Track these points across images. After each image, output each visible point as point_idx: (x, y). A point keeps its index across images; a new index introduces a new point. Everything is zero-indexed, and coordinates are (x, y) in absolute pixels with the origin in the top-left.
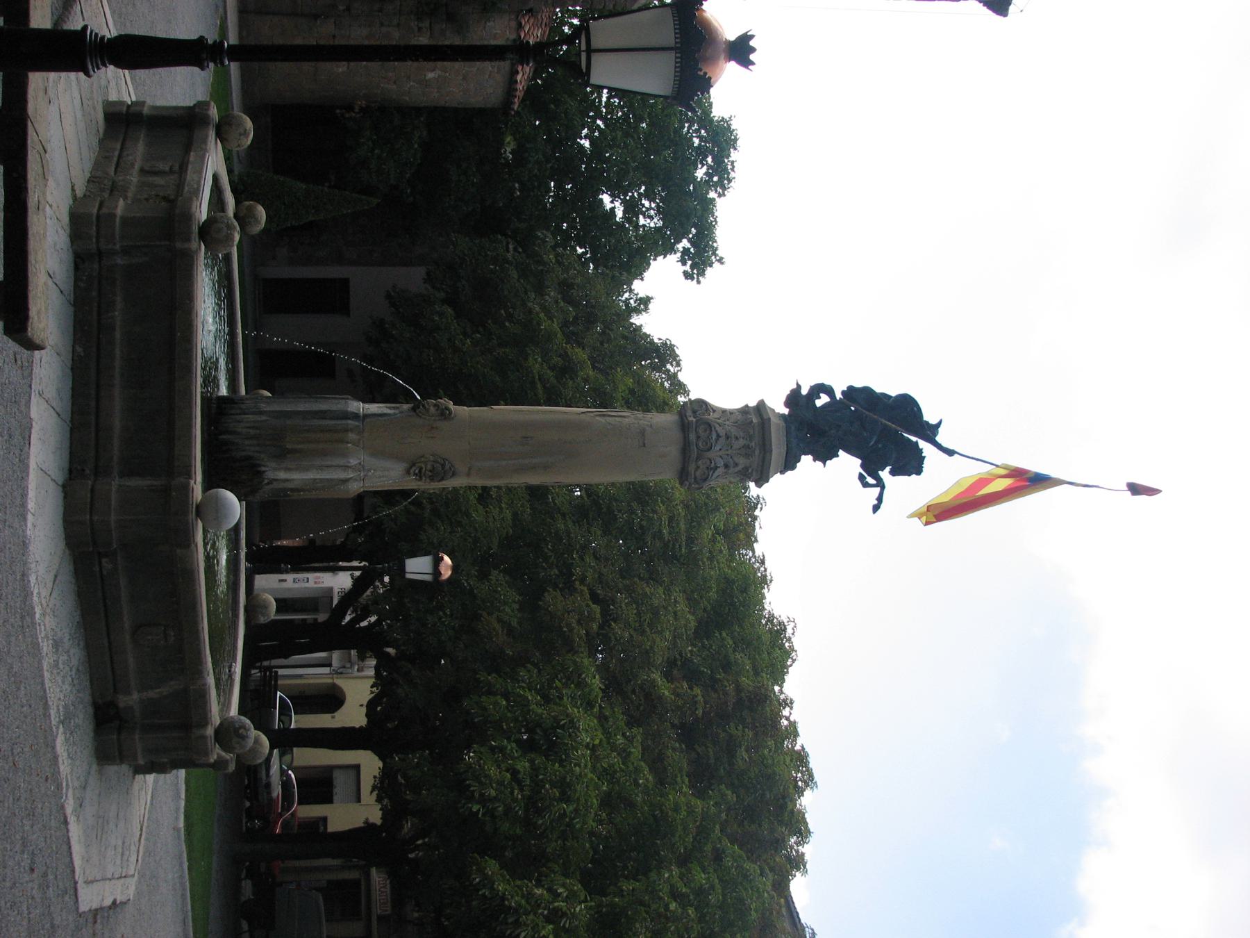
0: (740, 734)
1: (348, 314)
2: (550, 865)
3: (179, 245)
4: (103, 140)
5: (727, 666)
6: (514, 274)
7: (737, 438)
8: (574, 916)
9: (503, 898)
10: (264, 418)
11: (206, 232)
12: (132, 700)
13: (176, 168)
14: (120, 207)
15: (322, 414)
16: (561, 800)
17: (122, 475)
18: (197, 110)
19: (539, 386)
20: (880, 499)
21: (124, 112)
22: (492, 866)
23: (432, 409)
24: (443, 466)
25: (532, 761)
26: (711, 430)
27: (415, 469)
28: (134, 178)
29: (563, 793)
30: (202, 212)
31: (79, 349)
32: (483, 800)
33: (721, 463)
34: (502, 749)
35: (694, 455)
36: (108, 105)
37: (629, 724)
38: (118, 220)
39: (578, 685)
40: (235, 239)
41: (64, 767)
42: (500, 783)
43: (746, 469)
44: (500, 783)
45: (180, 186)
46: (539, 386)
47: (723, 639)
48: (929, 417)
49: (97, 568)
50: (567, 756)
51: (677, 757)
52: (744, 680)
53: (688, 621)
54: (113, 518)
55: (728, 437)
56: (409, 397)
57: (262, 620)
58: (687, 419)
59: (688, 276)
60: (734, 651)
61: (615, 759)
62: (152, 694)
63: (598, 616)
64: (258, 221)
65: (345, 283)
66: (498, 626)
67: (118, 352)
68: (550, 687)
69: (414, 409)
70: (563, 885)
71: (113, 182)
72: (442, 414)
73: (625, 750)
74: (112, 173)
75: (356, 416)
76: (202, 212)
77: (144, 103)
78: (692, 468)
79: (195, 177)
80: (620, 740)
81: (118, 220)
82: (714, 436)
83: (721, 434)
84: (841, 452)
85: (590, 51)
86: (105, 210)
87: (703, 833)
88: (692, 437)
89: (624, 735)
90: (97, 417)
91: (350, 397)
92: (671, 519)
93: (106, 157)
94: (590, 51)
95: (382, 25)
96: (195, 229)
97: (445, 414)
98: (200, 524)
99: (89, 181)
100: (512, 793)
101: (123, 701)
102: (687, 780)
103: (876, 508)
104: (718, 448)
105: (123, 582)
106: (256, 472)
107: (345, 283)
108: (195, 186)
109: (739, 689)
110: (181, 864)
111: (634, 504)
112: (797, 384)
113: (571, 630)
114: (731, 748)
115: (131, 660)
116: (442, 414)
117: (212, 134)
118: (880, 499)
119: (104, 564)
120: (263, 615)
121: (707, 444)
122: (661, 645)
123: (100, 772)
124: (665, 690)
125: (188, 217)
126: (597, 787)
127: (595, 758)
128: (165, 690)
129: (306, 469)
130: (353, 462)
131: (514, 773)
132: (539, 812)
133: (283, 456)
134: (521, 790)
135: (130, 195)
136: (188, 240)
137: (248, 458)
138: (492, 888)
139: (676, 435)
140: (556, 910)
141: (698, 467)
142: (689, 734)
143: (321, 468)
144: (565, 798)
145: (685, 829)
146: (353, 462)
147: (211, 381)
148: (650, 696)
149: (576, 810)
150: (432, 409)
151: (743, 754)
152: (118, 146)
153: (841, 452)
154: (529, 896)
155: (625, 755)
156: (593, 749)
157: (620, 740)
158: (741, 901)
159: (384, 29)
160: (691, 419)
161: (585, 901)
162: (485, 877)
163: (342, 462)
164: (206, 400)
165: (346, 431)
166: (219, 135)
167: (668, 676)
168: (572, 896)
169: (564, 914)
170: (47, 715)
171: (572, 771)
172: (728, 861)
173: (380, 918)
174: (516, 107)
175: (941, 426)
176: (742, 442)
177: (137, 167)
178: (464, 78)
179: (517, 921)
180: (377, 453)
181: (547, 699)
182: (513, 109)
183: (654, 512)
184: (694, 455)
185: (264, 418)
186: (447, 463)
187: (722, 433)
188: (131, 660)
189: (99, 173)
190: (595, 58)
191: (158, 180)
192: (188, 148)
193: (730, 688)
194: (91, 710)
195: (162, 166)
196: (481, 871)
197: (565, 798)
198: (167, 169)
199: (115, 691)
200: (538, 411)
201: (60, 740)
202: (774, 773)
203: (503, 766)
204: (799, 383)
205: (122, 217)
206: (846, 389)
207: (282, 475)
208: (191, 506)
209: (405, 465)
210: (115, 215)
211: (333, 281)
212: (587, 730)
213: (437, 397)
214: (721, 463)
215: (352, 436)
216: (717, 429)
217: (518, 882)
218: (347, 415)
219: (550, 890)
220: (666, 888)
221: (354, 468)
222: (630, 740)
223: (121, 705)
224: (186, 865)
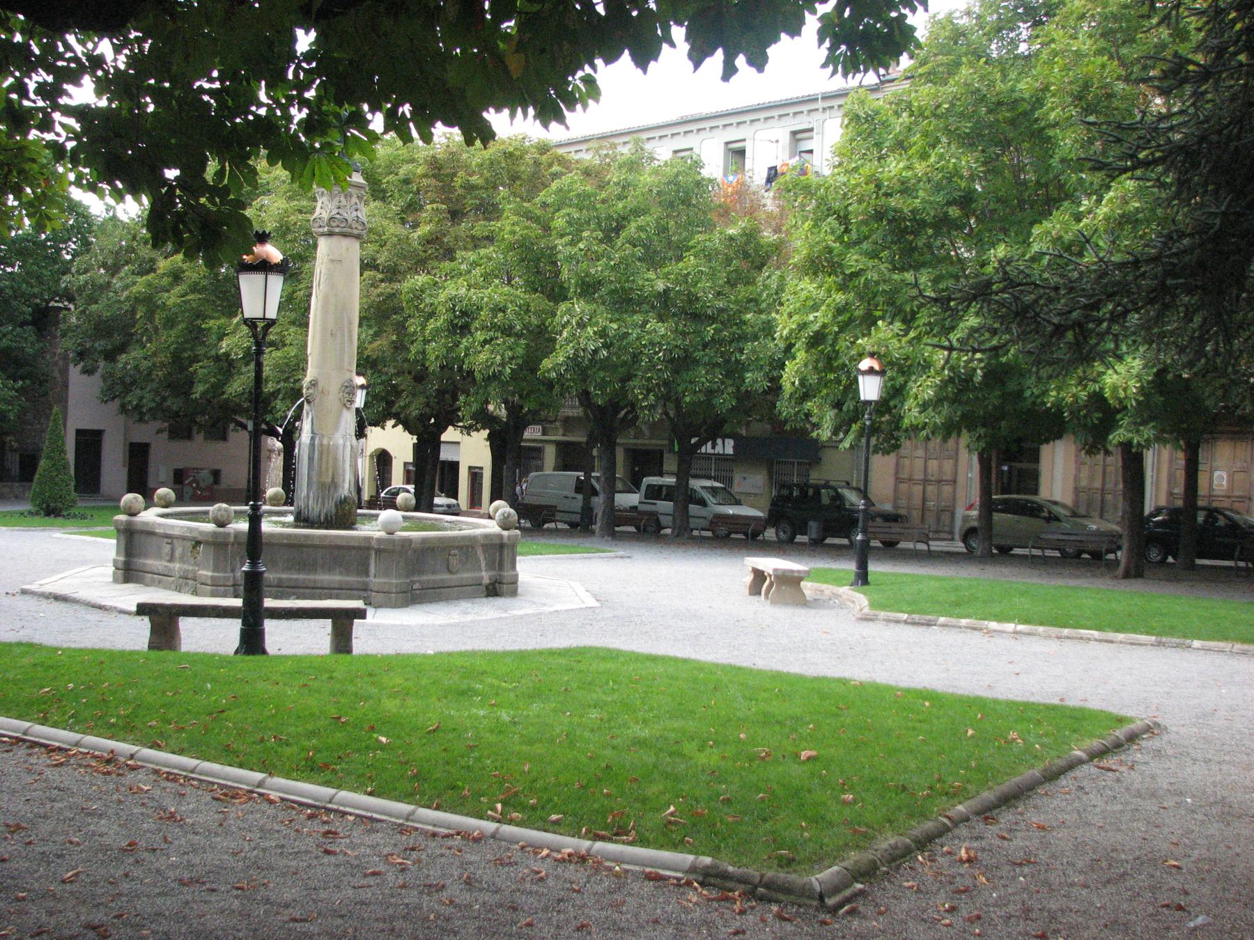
0: (460, 180)
1: (104, 431)
2: (547, 324)
3: (232, 539)
5: (407, 181)
6: (94, 307)
8: (582, 312)
9: (568, 358)
10: (311, 495)
11: (221, 524)
12: (486, 576)
13: (170, 541)
14: (206, 573)
15: (311, 459)
16: (504, 312)
17: (367, 575)
19: (189, 297)
22: (547, 363)
23: (311, 391)
24: (347, 387)
25: (477, 329)
27: (348, 404)
28: (177, 566)
29: (500, 310)
30: (210, 527)
32: (503, 365)
33: (355, 214)
34: (467, 349)
35: (349, 230)
36: (116, 581)
37: (453, 259)
38: (215, 574)
39: (422, 291)
41: (530, 611)
42: (492, 352)
43: (358, 197)
44: (492, 352)
45: (184, 538)
46: (189, 297)
47: (388, 182)
49: (418, 592)
50: (475, 305)
51: (480, 228)
52: (420, 171)
53: (376, 207)
54: (394, 581)
55: (339, 208)
56: (301, 407)
57: (414, 502)
60: (397, 174)
61: (477, 271)
62: (483, 564)
63: (372, 273)
64: (168, 494)
66: (375, 344)
67: (295, 576)
68: (423, 311)
69: (309, 402)
70: (562, 317)
72: (314, 385)
73: (471, 264)
75: (313, 439)
76: (210, 527)
77: (115, 561)
78: (356, 232)
79: (176, 529)
80: (463, 267)
81: (215, 574)
82: (338, 216)
85: (264, 319)
86: (209, 582)
87: (528, 216)
88: (337, 230)
89: (460, 264)
90: (335, 589)
92: (300, 212)
94: (264, 319)
96: (221, 530)
97: (314, 384)
98: (398, 533)
99: (180, 591)
100: (499, 345)
101: (486, 581)
102: (492, 223)
105: (424, 578)
106: (343, 502)
109: (425, 176)
110: (539, 559)
111: (289, 237)
113: (382, 294)
114: (470, 188)
115: (466, 575)
116: (314, 385)
117: (136, 519)
122: (394, 230)
123: (522, 595)
124: (424, 230)
125: (215, 534)
126: (496, 286)
127: (475, 286)
128: (482, 558)
129: (344, 471)
130: (341, 442)
131: (486, 342)
132: (511, 327)
133: (334, 485)
134: (497, 338)
136: (228, 534)
137: (336, 505)
138: (561, 365)
139: (335, 240)
140: (578, 324)
142: (455, 215)
143: (344, 461)
144: (503, 310)
145: (527, 228)
146: (341, 442)
147: (284, 525)
148: (430, 241)
149: (511, 302)
150: (311, 391)
151: (475, 179)
152: (150, 575)
154: (568, 341)
155: (475, 264)
156: (470, 286)
157: (463, 267)
158: (578, 196)
161: (573, 304)
162: (553, 368)
163: (341, 448)
164: (296, 527)
165: (321, 445)
166: (134, 515)
167: (415, 226)
168: (569, 312)
169: (581, 318)
170: (506, 618)
171: (487, 303)
172: (550, 200)
173: (544, 434)
176: (342, 199)
177: (166, 564)
179: (583, 350)
180: (336, 427)
181: (432, 314)
183: (295, 223)
184: (349, 230)
185: (311, 495)
187: (337, 211)
188: (466, 575)
189: (173, 587)
190: (267, 316)
192: (151, 533)
193: (425, 182)
194: (491, 599)
195: (167, 548)
196: (548, 371)
197: (503, 310)
198: (169, 546)
199: (480, 585)
200: (314, 327)
201: (515, 612)
202: (490, 159)
203: (479, 348)
205: (213, 571)
207: (347, 485)
209: (345, 411)
210: (212, 577)
211: (78, 443)
212: (456, 289)
213: (301, 388)
214: (355, 214)
215: (325, 442)
217: (558, 347)
218: (312, 444)
219: (564, 327)
220: (569, 248)
221: (345, 441)
222: (464, 259)
224: (539, 556)
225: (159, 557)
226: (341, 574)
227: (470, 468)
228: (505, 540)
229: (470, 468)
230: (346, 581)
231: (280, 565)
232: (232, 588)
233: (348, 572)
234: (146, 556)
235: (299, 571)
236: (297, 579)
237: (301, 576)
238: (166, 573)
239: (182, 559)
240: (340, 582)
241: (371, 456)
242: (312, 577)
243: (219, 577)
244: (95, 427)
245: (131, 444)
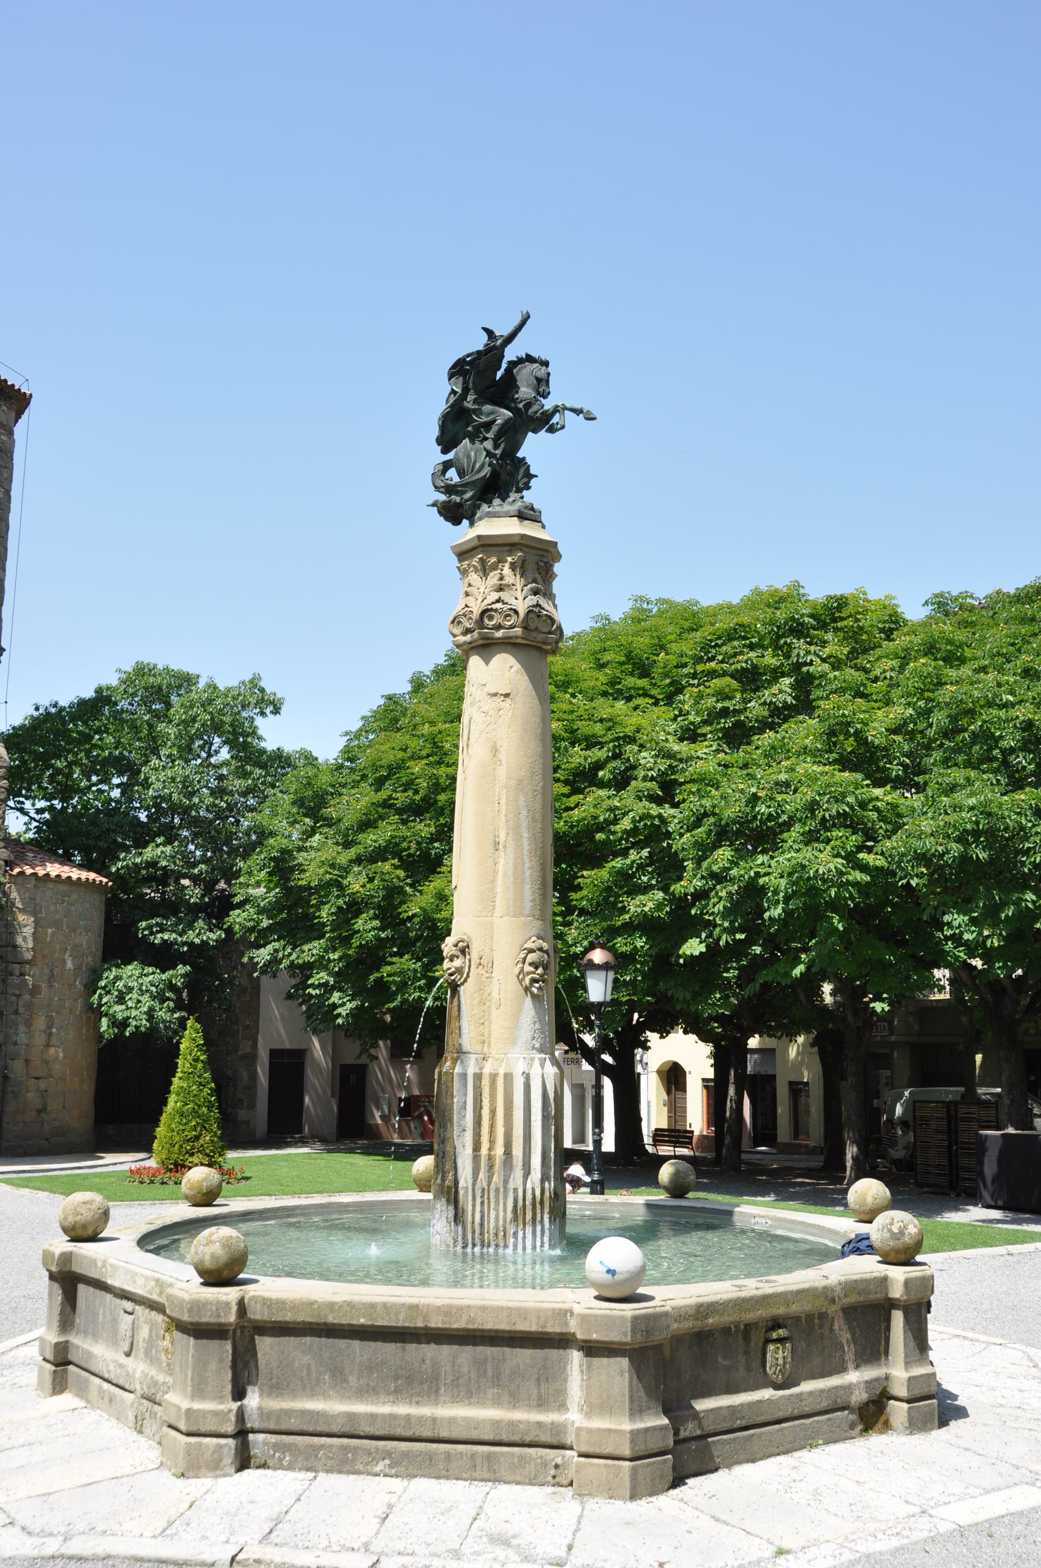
4: (88, 1401)
7: (501, 579)
17: (562, 1406)
18: (54, 1269)
20: (578, 412)
21: (53, 1368)
23: (457, 963)
26: (496, 610)
31: (380, 1467)
40: (228, 1235)
48: (480, 342)
55: (500, 589)
58: (475, 641)
59: (276, 711)
65: (274, 1054)
71: (143, 1397)
74: (132, 1396)
83: (497, 597)
84: (520, 455)
91: (437, 1071)
93: (110, 1401)
95: (16, 1012)
103: (590, 418)
104: (514, 602)
107: (274, 1054)
108: (153, 1283)
112: (434, 505)
118: (578, 412)
119: (687, 1434)
120: (687, 1176)
121: (509, 615)
135: (161, 1378)
141: (536, 629)
153: (520, 455)
159: (21, 1010)
160: (476, 634)
174: (105, 880)
175: (490, 328)
178: (74, 931)
182: (107, 883)
186: (526, 946)
187: (495, 596)
189: (679, 1095)
191: (144, 1332)
204: (431, 502)
206: (440, 448)
208: (614, 1312)
216: (490, 602)
223: (865, 1396)
225: (113, 1341)
226: (497, 1403)
227: (791, 1083)
228: (897, 1292)
229: (791, 1083)
230: (512, 1424)
231: (353, 1380)
232: (231, 1442)
233: (514, 1401)
234: (96, 1336)
235: (397, 1394)
236: (393, 1417)
237: (403, 1409)
238: (121, 1382)
239: (150, 1358)
240: (496, 1423)
241: (659, 1072)
242: (426, 1411)
243: (204, 1414)
244: (296, 1046)
245: (342, 1066)
